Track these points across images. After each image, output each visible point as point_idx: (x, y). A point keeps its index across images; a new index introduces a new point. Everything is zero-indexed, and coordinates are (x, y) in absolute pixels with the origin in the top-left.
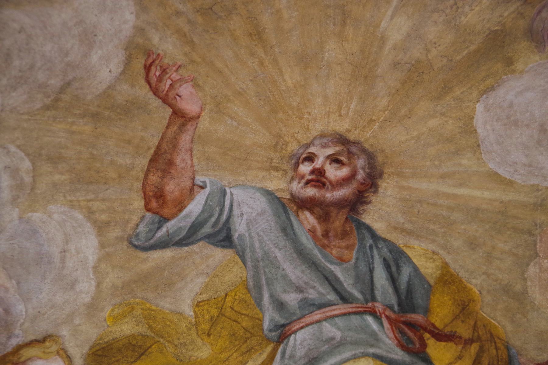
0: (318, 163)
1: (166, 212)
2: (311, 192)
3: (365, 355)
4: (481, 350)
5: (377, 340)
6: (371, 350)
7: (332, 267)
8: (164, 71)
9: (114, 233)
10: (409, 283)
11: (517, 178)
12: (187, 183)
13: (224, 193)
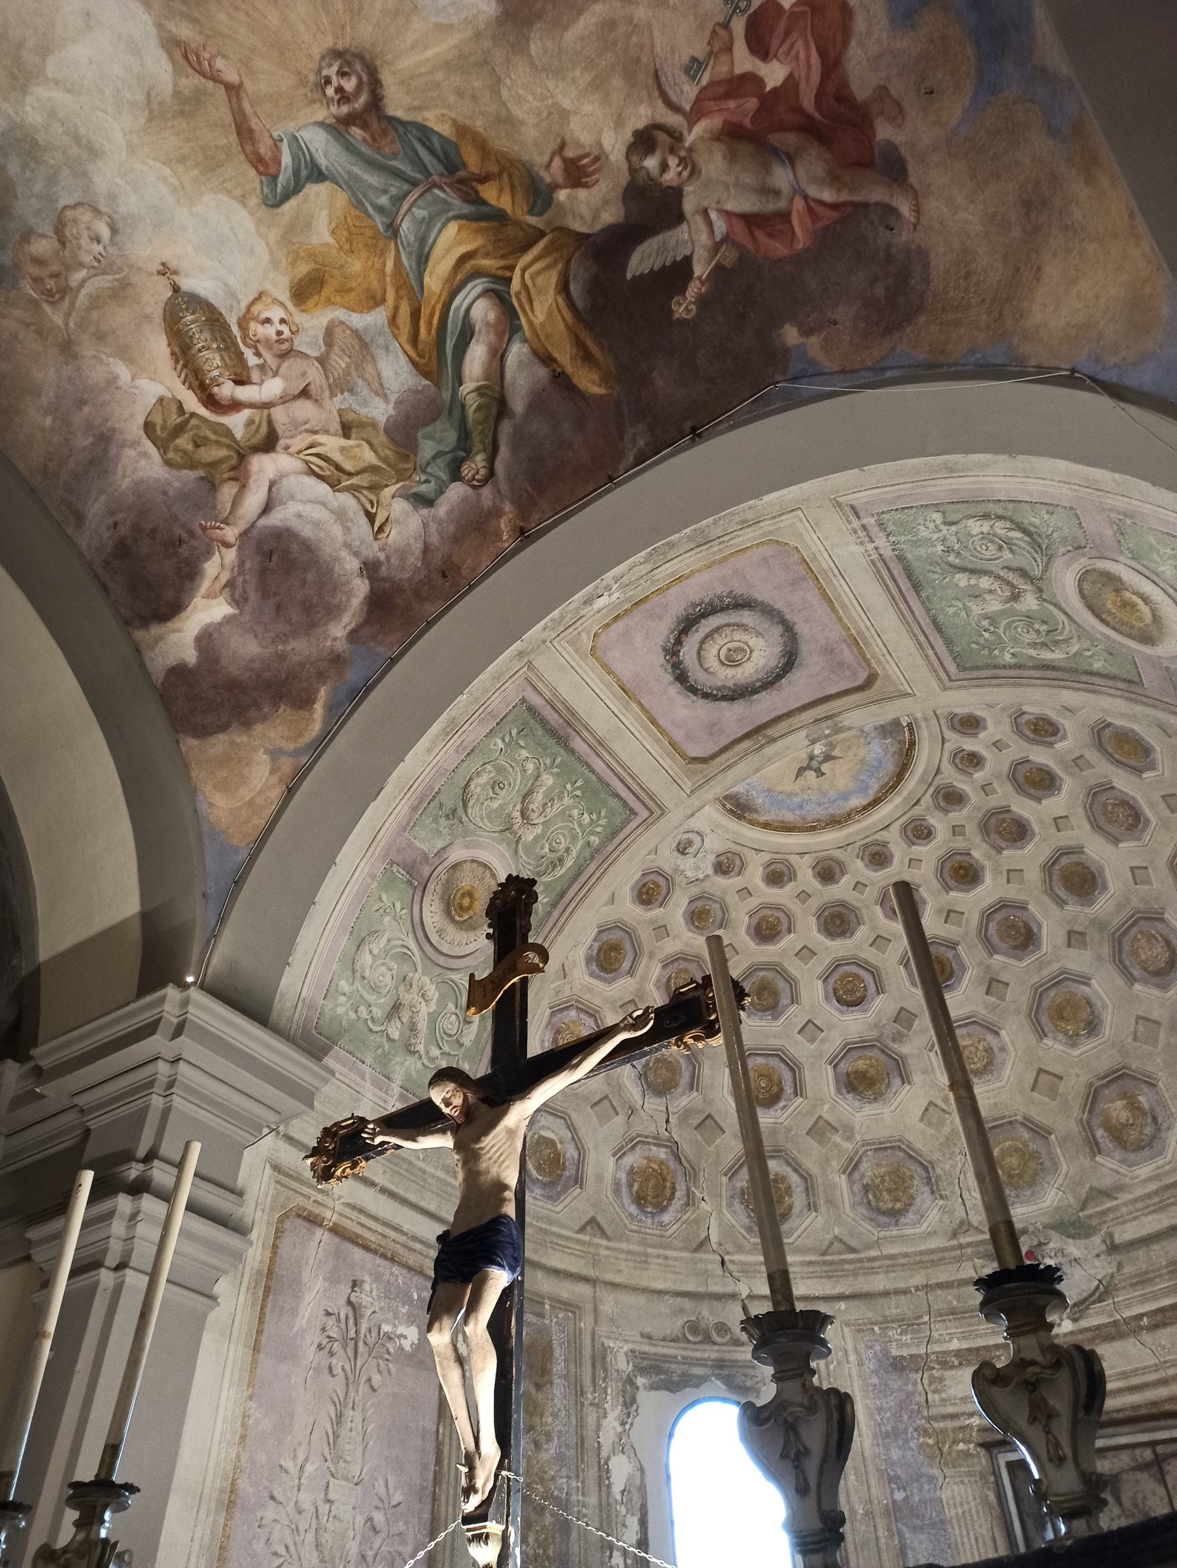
1: (272, 170)
2: (345, 109)
3: (448, 220)
4: (510, 176)
5: (449, 204)
6: (450, 214)
7: (392, 163)
8: (198, 56)
10: (443, 150)
11: (454, 20)
12: (270, 142)
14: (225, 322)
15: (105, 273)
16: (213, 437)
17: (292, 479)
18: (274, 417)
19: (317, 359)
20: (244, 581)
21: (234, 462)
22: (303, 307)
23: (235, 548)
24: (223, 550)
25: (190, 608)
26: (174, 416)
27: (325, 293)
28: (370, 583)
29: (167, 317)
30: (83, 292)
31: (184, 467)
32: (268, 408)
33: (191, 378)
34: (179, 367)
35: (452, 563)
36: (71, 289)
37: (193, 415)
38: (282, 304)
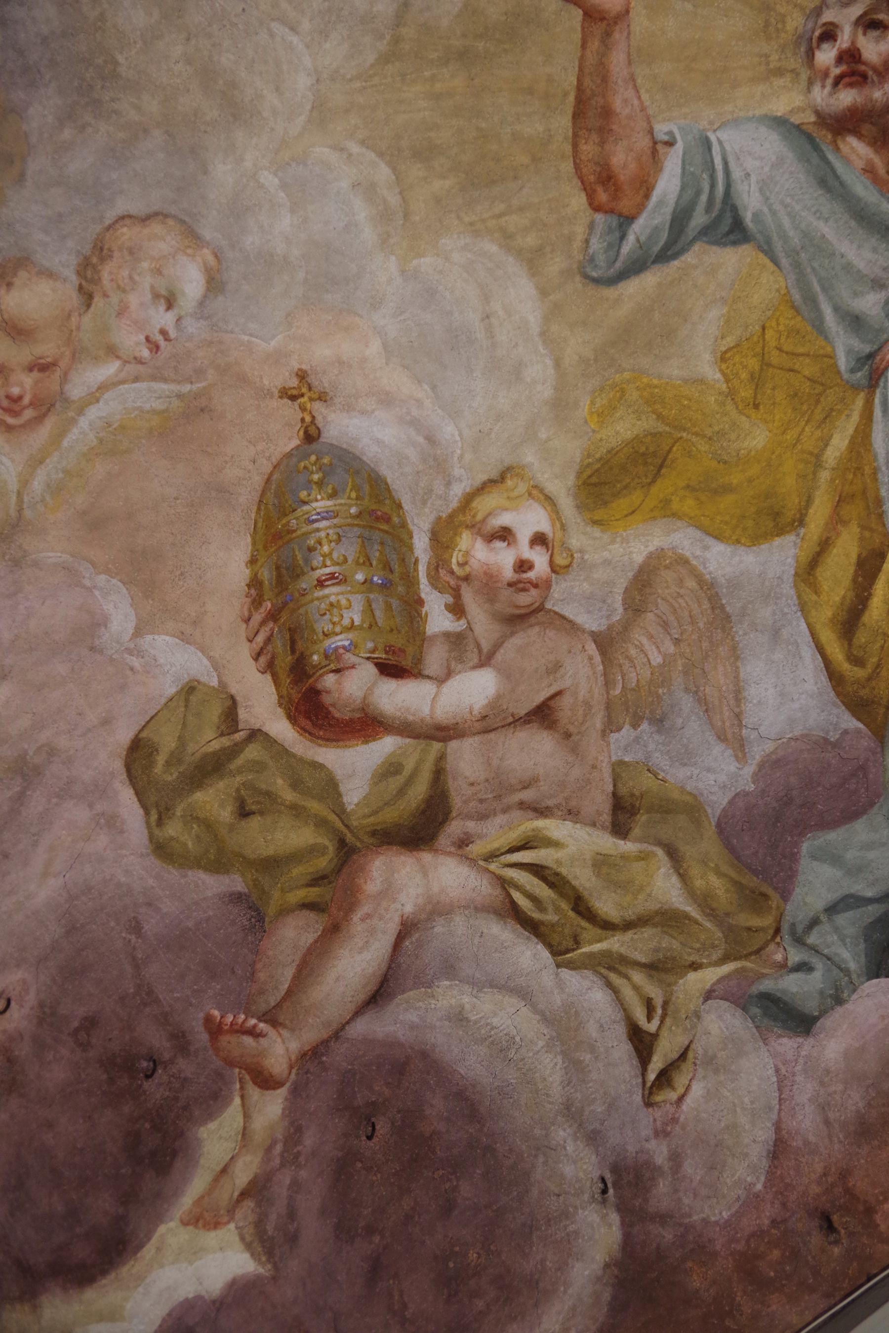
0: (844, 40)
2: (847, 97)
9: (555, 265)
12: (644, 143)
13: (707, 145)
14: (404, 525)
15: (154, 378)
16: (289, 796)
17: (459, 925)
18: (450, 763)
19: (596, 637)
20: (296, 1186)
21: (323, 863)
22: (599, 514)
23: (283, 1092)
24: (254, 1093)
25: (148, 1252)
26: (209, 733)
27: (659, 490)
28: (625, 1225)
29: (270, 497)
30: (94, 413)
31: (198, 863)
32: (445, 740)
33: (279, 645)
34: (257, 617)
35: (848, 1191)
36: (66, 400)
37: (255, 734)
38: (549, 501)
